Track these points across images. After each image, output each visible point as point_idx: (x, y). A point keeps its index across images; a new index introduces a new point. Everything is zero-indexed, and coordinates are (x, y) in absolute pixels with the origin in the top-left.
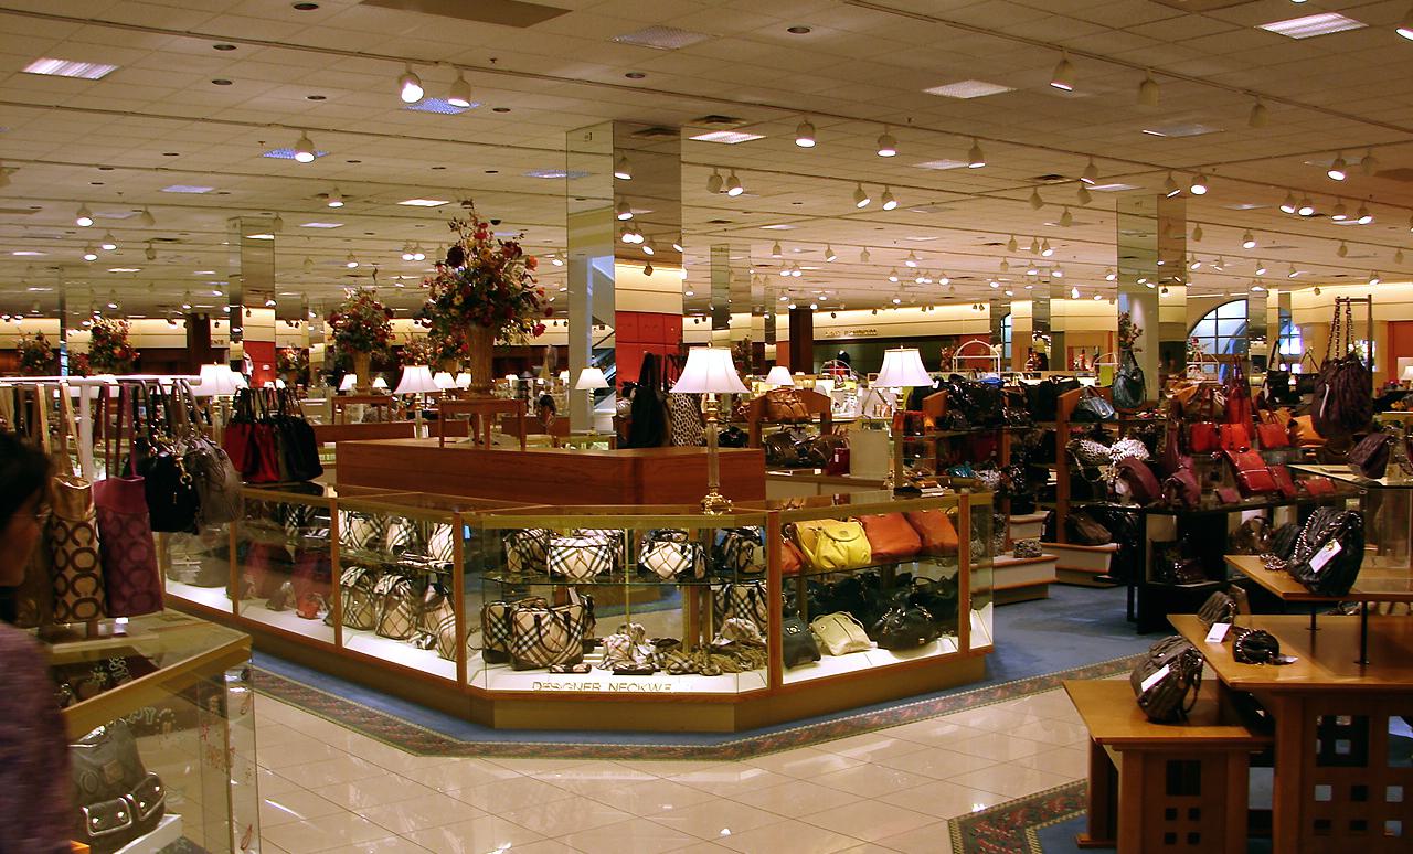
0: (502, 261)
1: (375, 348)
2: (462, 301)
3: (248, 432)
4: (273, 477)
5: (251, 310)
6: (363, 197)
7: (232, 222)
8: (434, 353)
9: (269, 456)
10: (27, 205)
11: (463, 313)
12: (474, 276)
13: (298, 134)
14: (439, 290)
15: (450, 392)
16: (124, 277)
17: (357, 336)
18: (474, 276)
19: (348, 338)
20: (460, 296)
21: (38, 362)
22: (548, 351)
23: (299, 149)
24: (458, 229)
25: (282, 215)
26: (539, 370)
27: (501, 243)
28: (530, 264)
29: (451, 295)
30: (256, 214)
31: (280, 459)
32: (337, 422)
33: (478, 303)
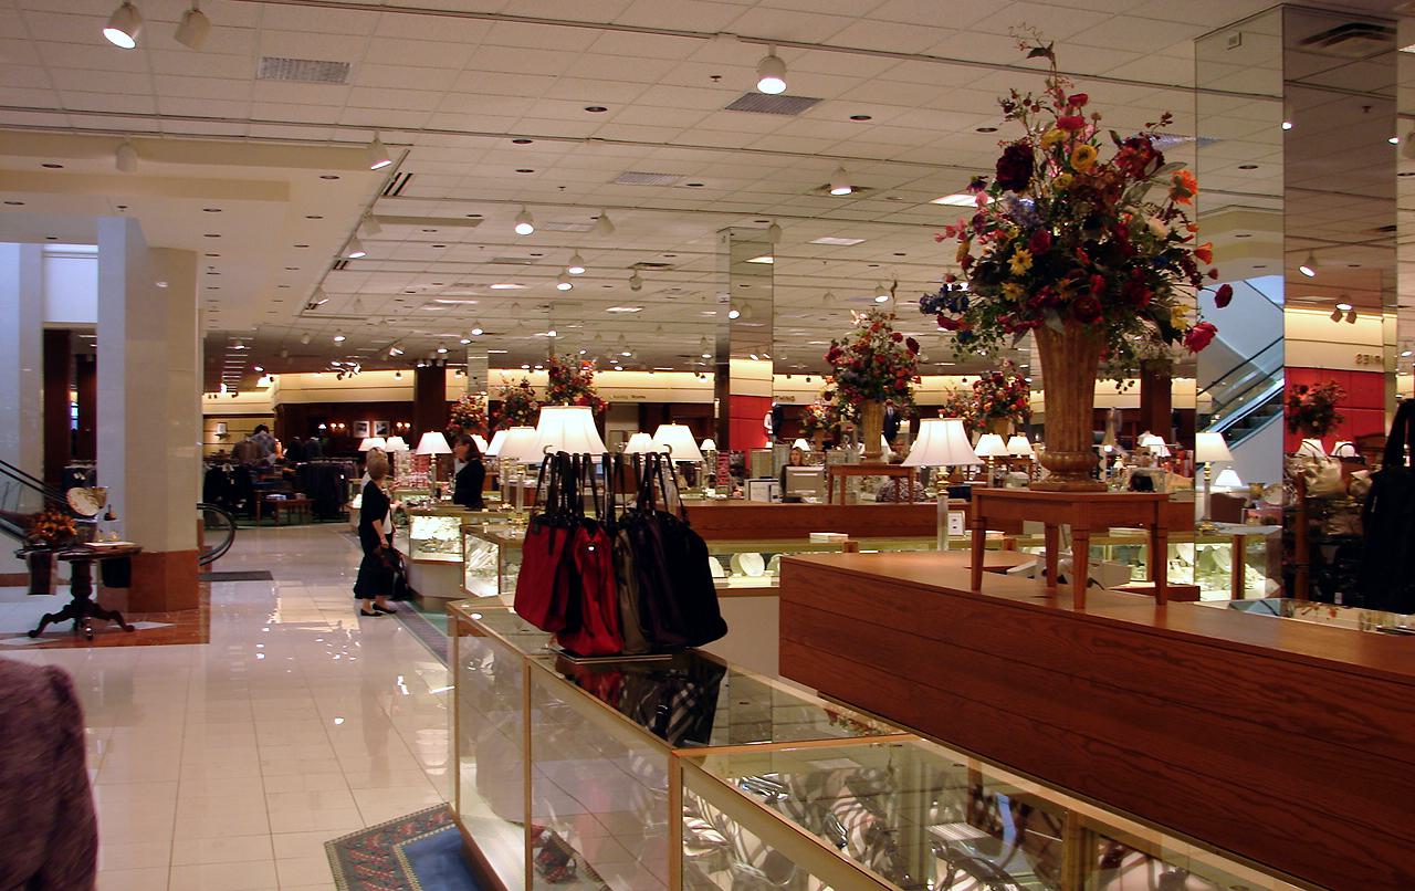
0: (1121, 178)
1: (892, 395)
2: (1029, 264)
3: (559, 545)
4: (610, 644)
5: (810, 377)
6: (884, 191)
7: (721, 235)
8: (981, 410)
9: (600, 596)
10: (460, 212)
11: (1032, 293)
12: (1055, 213)
13: (763, 51)
14: (980, 250)
15: (1000, 460)
16: (626, 318)
17: (866, 378)
18: (1055, 213)
19: (854, 381)
20: (1024, 253)
21: (520, 413)
22: (1112, 414)
23: (764, 73)
24: (1021, 115)
25: (780, 222)
26: (1103, 437)
27: (1117, 142)
28: (1182, 190)
29: (1006, 252)
30: (749, 222)
31: (626, 606)
32: (836, 502)
33: (1065, 268)
